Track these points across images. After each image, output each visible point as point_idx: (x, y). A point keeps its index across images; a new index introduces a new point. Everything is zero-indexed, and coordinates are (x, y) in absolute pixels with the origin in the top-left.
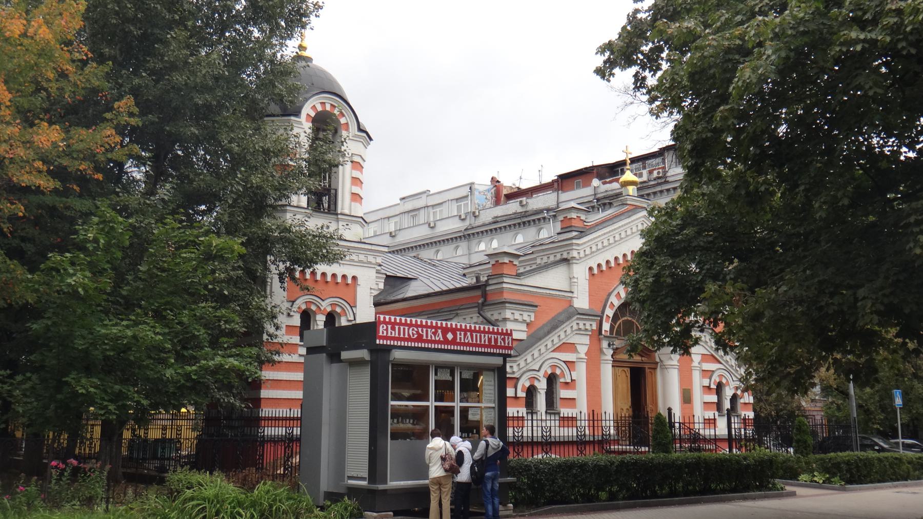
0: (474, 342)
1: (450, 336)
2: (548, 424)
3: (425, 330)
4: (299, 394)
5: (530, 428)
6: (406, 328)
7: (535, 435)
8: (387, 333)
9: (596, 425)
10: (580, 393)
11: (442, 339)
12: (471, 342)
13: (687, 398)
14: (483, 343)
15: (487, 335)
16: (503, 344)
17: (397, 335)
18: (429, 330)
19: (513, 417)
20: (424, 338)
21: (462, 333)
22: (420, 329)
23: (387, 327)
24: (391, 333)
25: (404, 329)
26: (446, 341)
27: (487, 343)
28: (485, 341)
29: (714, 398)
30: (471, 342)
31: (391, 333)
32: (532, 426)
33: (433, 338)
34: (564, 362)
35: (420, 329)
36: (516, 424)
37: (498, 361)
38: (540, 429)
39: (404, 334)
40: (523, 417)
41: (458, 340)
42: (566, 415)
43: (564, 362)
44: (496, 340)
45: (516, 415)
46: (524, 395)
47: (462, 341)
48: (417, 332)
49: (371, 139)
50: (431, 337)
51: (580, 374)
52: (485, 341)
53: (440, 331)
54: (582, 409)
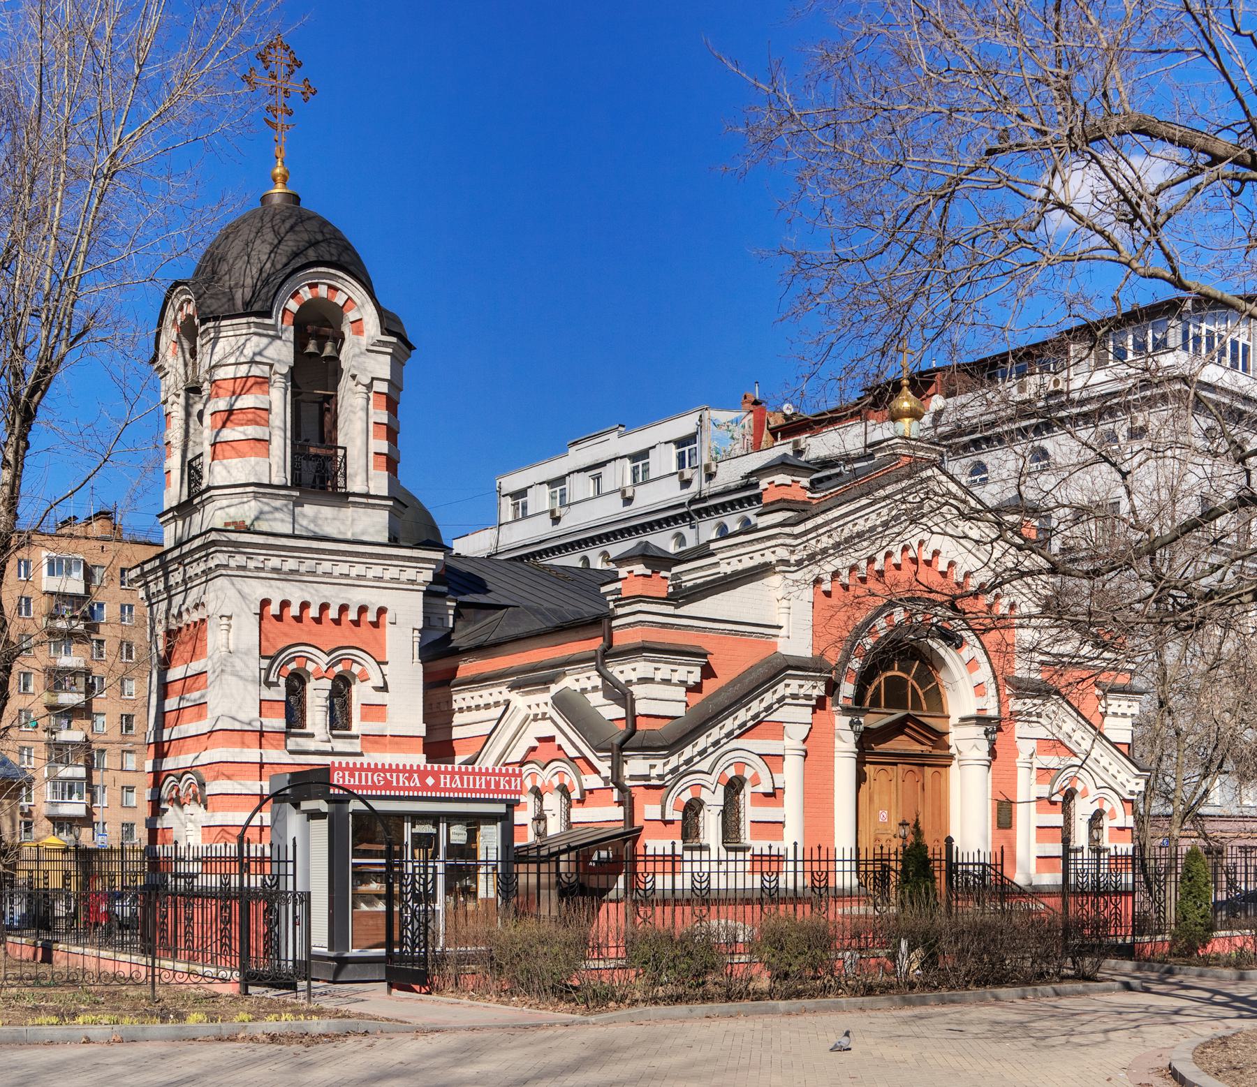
0: (465, 786)
1: (430, 781)
2: (824, 868)
3: (395, 775)
4: (384, 869)
5: (791, 876)
6: (370, 774)
7: (800, 884)
8: (344, 781)
9: (1243, 876)
10: (791, 810)
11: (418, 785)
12: (460, 786)
13: (1004, 815)
14: (478, 787)
15: (484, 778)
16: (507, 788)
17: (357, 783)
18: (401, 775)
19: (762, 855)
20: (395, 784)
21: (448, 777)
22: (388, 775)
23: (344, 774)
24: (349, 781)
25: (367, 775)
26: (425, 787)
27: (483, 787)
28: (481, 785)
29: (1058, 819)
30: (460, 786)
31: (349, 781)
32: (795, 872)
33: (407, 784)
34: (760, 755)
35: (388, 775)
36: (766, 868)
37: (501, 808)
38: (808, 875)
39: (367, 782)
40: (673, 855)
41: (442, 785)
42: (659, 852)
43: (760, 755)
44: (497, 784)
45: (766, 852)
46: (678, 816)
47: (448, 786)
48: (385, 778)
49: (410, 347)
50: (404, 783)
51: (791, 776)
52: (481, 785)
53: (416, 776)
54: (792, 837)
